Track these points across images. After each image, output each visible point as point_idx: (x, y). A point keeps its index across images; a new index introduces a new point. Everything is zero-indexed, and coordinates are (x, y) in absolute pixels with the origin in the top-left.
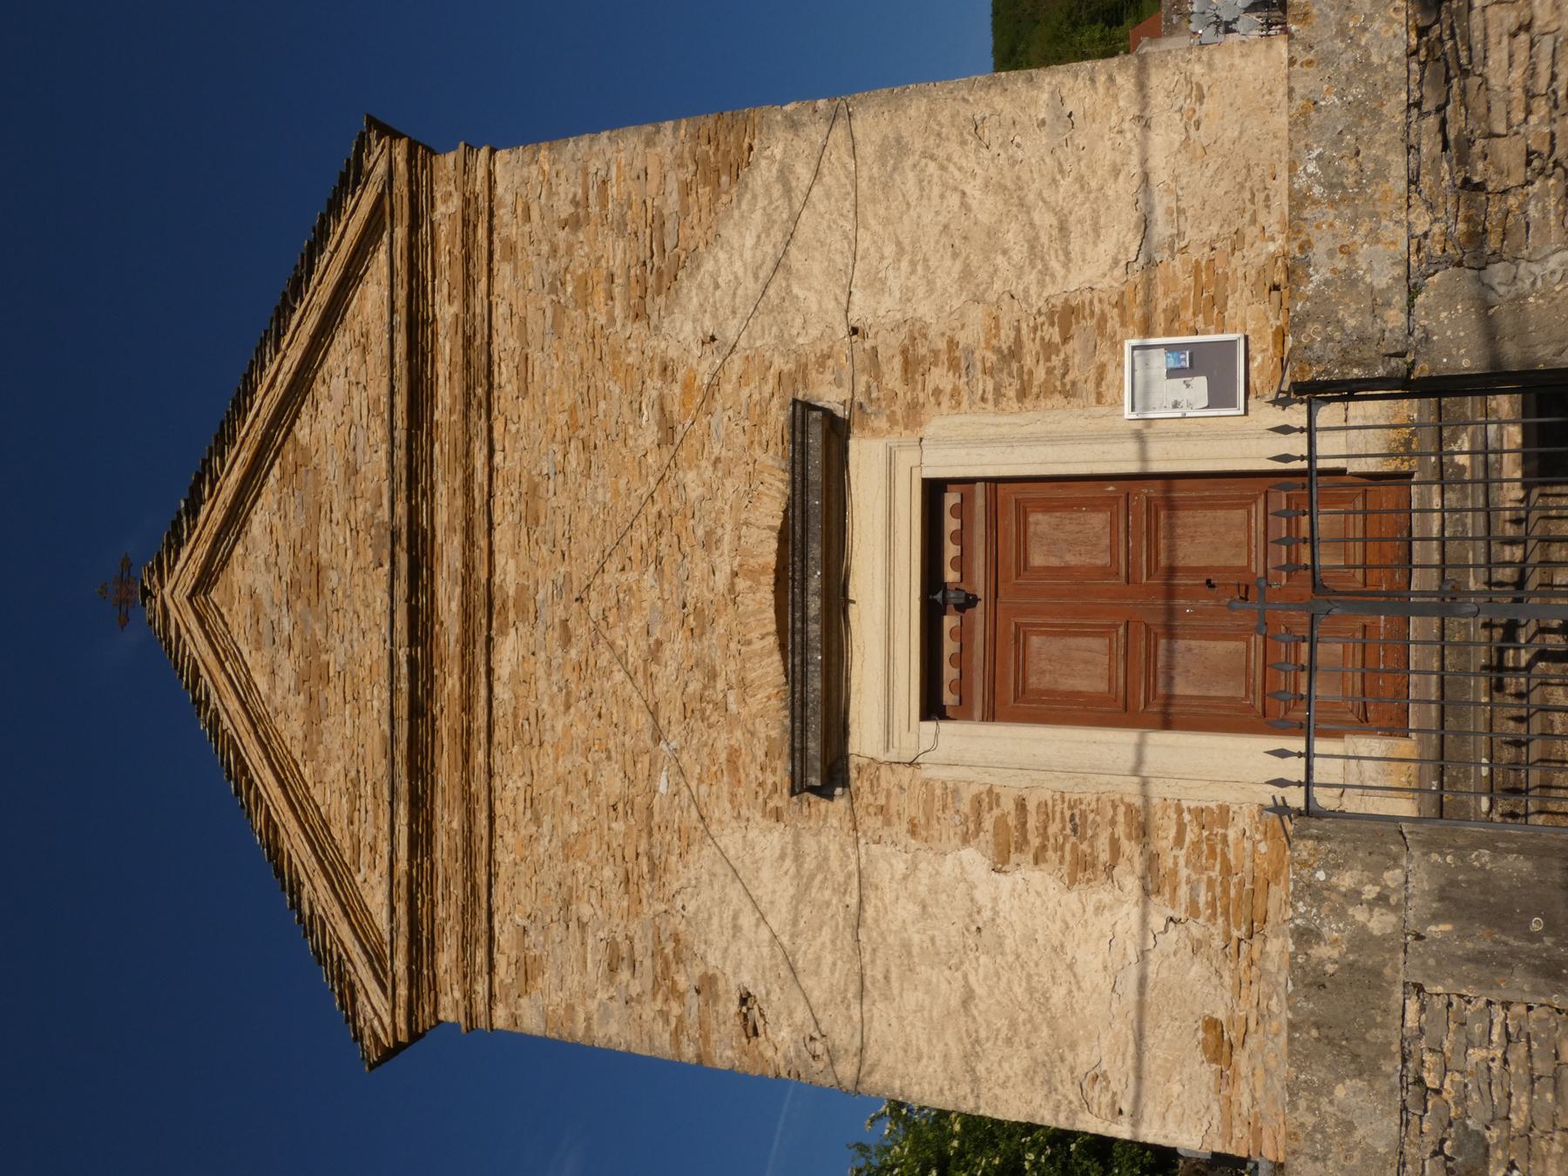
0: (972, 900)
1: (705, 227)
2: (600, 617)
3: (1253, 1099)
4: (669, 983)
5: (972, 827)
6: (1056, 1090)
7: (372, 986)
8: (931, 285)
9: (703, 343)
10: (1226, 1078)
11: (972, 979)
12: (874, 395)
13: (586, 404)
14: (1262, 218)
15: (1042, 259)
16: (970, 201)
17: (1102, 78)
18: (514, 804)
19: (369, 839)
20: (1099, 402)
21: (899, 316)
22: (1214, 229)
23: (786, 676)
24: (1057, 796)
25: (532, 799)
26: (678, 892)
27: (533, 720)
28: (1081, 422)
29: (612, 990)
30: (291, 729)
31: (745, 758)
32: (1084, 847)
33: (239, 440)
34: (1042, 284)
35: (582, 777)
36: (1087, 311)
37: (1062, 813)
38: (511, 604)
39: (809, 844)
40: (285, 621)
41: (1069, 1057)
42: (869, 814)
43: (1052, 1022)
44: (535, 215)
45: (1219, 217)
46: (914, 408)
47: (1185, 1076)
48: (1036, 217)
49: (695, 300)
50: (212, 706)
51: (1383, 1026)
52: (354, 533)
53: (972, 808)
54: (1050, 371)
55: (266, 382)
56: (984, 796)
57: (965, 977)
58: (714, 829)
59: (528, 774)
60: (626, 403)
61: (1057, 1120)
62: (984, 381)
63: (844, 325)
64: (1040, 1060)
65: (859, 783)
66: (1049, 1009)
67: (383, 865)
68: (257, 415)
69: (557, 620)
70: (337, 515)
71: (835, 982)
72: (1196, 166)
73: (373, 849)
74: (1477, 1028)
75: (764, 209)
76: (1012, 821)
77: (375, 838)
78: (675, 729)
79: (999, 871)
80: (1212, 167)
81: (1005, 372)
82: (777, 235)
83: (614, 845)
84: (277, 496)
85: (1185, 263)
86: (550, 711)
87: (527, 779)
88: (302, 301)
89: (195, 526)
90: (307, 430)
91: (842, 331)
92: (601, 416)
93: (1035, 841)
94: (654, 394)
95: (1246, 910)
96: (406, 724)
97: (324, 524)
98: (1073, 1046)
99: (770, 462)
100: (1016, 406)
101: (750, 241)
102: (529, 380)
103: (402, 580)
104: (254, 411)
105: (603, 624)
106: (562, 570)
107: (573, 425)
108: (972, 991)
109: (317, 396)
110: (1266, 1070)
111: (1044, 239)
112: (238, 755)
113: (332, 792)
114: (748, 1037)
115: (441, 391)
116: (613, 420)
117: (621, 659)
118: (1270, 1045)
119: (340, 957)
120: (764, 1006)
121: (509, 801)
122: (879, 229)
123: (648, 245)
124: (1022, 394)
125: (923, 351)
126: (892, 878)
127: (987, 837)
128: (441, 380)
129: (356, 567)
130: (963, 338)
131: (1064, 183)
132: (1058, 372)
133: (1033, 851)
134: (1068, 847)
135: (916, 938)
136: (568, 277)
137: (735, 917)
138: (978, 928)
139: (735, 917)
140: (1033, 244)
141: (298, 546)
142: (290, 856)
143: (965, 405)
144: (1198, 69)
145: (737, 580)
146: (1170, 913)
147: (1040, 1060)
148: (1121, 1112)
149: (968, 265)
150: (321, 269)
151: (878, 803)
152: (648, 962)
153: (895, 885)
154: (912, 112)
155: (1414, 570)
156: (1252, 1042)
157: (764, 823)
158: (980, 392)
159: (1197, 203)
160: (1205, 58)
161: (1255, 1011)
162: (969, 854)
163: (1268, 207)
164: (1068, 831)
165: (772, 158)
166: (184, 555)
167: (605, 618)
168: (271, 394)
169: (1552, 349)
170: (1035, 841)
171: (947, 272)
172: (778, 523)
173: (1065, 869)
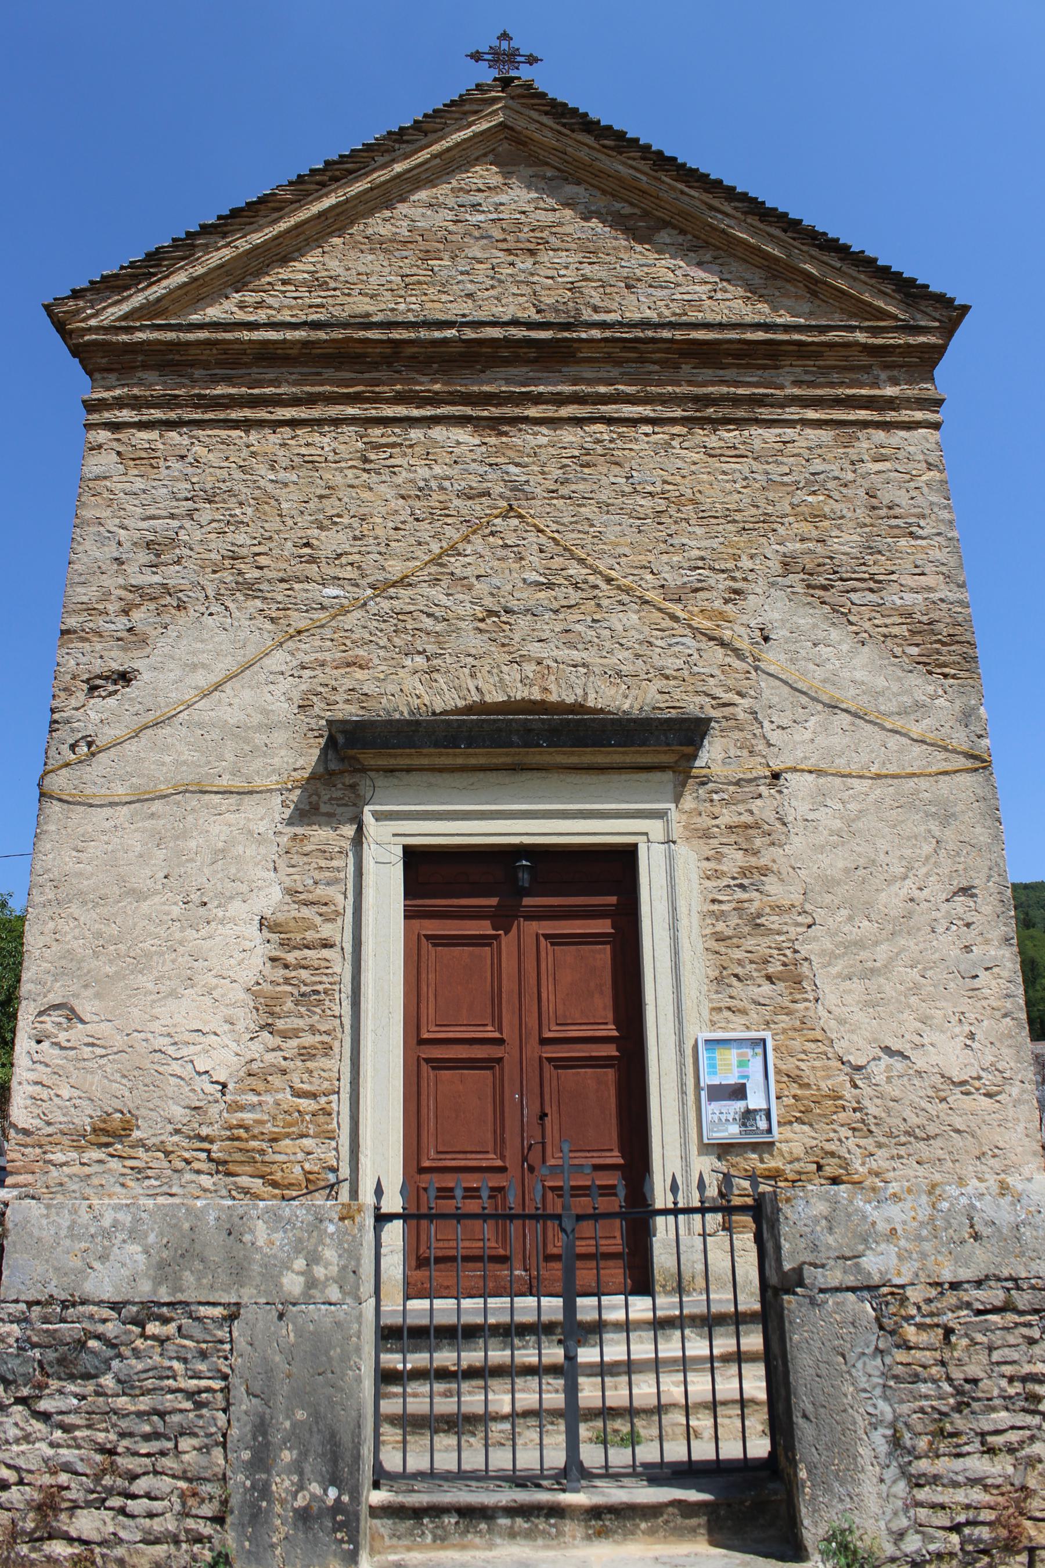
0: (231, 898)
1: (871, 630)
2: (494, 529)
3: (62, 1165)
4: (138, 601)
5: (302, 897)
6: (56, 980)
7: (125, 308)
8: (821, 849)
9: (762, 629)
10: (79, 1140)
11: (157, 899)
12: (715, 797)
13: (701, 515)
14: (881, 1153)
15: (845, 954)
16: (898, 885)
17: (1009, 1005)
18: (308, 445)
19: (270, 301)
20: (713, 1009)
21: (791, 819)
22: (872, 1110)
23: (441, 714)
24: (337, 979)
25: (312, 462)
26: (227, 608)
27: (389, 462)
28: (694, 993)
29: (129, 544)
30: (378, 225)
31: (359, 674)
32: (289, 1005)
33: (660, 174)
34: (823, 953)
35: (335, 512)
36: (798, 997)
37: (321, 983)
38: (504, 439)
39: (279, 737)
40: (481, 217)
41: (89, 992)
42: (310, 796)
43: (119, 976)
44: (879, 466)
45: (883, 1115)
46: (706, 835)
47: (78, 1102)
48: (884, 947)
49: (802, 621)
50: (397, 146)
51: (199, 1286)
52: (569, 286)
53: (320, 896)
54: (740, 963)
55: (716, 203)
56: (333, 908)
57: (156, 893)
58: (290, 645)
59: (337, 458)
60: (702, 553)
61: (27, 981)
62: (729, 901)
63: (782, 766)
64: (83, 964)
65: (340, 786)
66: (132, 972)
67: (241, 316)
68: (682, 192)
69: (489, 485)
70: (587, 269)
71: (146, 764)
72: (931, 1093)
73: (260, 305)
74: (202, 1367)
75: (888, 688)
76: (310, 935)
77: (270, 307)
78: (386, 605)
79: (261, 924)
80: (928, 1106)
81: (740, 921)
82: (864, 702)
83: (272, 545)
84: (604, 211)
85: (842, 1084)
86: (399, 480)
87: (331, 457)
88: (794, 239)
89: (573, 131)
90: (668, 241)
91: (776, 765)
92: (690, 529)
93: (291, 957)
94: (712, 582)
95: (238, 1156)
96: (384, 337)
97: (579, 257)
98: (98, 996)
99: (649, 696)
100: (708, 931)
101: (859, 675)
102: (723, 459)
103: (526, 333)
104: (686, 190)
105: (487, 531)
106: (538, 490)
107: (679, 502)
108: (146, 899)
109: (701, 252)
110: (89, 1176)
111: (864, 955)
112: (351, 172)
113: (314, 264)
114: (89, 679)
115: (710, 371)
116: (685, 541)
117: (453, 550)
118: (112, 1180)
119: (154, 275)
120: (118, 696)
121: (310, 440)
122: (872, 797)
123: (853, 576)
124: (720, 938)
125: (758, 842)
126: (249, 820)
127: (295, 911)
128: (721, 372)
129: (538, 288)
130: (771, 885)
131: (914, 974)
132: (739, 970)
133: (283, 955)
134: (289, 988)
135: (192, 844)
136: (821, 498)
137: (204, 666)
138: (205, 904)
139: (204, 666)
140: (859, 944)
141: (554, 230)
142: (252, 223)
143: (709, 884)
144: (1015, 1091)
145: (534, 663)
146: (231, 1086)
147: (83, 964)
148: (39, 1042)
149: (839, 884)
150: (825, 258)
151: (322, 805)
152: (157, 579)
153: (242, 822)
154: (979, 830)
155: (481, 1300)
156: (114, 1164)
157: (296, 695)
158: (721, 898)
159: (897, 1093)
160: (1025, 1096)
161: (144, 1165)
162: (276, 894)
163: (892, 1158)
164: (303, 989)
165: (934, 697)
166: (545, 119)
167: (492, 534)
168: (704, 207)
169: (809, 1409)
170: (291, 957)
171: (835, 863)
172: (590, 703)
173: (266, 987)
